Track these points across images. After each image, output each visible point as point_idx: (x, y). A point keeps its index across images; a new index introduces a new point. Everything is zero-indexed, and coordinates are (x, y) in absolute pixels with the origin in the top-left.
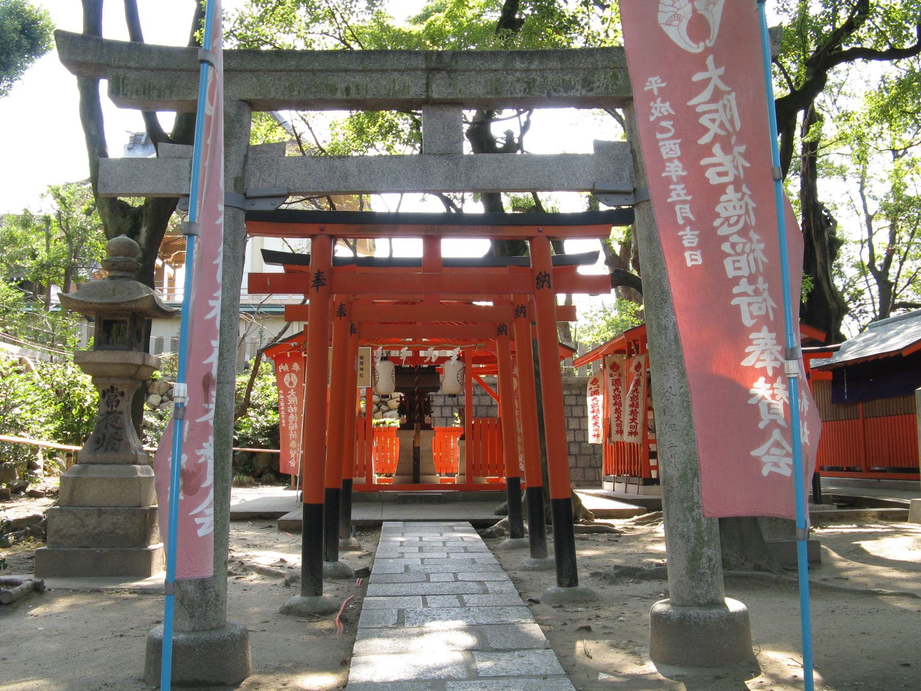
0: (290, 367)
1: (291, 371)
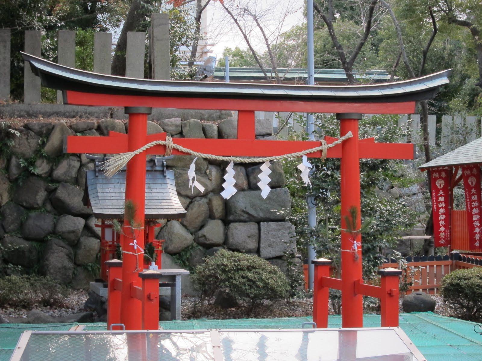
0: (440, 175)
1: (441, 178)
